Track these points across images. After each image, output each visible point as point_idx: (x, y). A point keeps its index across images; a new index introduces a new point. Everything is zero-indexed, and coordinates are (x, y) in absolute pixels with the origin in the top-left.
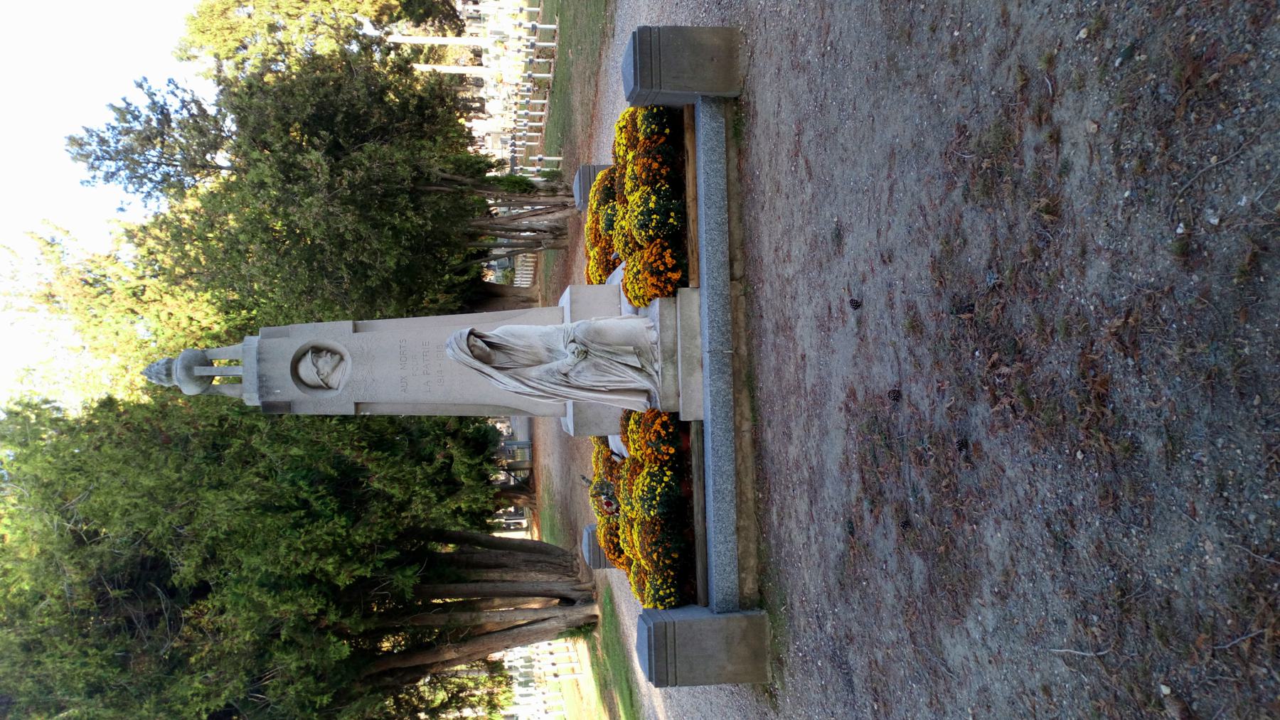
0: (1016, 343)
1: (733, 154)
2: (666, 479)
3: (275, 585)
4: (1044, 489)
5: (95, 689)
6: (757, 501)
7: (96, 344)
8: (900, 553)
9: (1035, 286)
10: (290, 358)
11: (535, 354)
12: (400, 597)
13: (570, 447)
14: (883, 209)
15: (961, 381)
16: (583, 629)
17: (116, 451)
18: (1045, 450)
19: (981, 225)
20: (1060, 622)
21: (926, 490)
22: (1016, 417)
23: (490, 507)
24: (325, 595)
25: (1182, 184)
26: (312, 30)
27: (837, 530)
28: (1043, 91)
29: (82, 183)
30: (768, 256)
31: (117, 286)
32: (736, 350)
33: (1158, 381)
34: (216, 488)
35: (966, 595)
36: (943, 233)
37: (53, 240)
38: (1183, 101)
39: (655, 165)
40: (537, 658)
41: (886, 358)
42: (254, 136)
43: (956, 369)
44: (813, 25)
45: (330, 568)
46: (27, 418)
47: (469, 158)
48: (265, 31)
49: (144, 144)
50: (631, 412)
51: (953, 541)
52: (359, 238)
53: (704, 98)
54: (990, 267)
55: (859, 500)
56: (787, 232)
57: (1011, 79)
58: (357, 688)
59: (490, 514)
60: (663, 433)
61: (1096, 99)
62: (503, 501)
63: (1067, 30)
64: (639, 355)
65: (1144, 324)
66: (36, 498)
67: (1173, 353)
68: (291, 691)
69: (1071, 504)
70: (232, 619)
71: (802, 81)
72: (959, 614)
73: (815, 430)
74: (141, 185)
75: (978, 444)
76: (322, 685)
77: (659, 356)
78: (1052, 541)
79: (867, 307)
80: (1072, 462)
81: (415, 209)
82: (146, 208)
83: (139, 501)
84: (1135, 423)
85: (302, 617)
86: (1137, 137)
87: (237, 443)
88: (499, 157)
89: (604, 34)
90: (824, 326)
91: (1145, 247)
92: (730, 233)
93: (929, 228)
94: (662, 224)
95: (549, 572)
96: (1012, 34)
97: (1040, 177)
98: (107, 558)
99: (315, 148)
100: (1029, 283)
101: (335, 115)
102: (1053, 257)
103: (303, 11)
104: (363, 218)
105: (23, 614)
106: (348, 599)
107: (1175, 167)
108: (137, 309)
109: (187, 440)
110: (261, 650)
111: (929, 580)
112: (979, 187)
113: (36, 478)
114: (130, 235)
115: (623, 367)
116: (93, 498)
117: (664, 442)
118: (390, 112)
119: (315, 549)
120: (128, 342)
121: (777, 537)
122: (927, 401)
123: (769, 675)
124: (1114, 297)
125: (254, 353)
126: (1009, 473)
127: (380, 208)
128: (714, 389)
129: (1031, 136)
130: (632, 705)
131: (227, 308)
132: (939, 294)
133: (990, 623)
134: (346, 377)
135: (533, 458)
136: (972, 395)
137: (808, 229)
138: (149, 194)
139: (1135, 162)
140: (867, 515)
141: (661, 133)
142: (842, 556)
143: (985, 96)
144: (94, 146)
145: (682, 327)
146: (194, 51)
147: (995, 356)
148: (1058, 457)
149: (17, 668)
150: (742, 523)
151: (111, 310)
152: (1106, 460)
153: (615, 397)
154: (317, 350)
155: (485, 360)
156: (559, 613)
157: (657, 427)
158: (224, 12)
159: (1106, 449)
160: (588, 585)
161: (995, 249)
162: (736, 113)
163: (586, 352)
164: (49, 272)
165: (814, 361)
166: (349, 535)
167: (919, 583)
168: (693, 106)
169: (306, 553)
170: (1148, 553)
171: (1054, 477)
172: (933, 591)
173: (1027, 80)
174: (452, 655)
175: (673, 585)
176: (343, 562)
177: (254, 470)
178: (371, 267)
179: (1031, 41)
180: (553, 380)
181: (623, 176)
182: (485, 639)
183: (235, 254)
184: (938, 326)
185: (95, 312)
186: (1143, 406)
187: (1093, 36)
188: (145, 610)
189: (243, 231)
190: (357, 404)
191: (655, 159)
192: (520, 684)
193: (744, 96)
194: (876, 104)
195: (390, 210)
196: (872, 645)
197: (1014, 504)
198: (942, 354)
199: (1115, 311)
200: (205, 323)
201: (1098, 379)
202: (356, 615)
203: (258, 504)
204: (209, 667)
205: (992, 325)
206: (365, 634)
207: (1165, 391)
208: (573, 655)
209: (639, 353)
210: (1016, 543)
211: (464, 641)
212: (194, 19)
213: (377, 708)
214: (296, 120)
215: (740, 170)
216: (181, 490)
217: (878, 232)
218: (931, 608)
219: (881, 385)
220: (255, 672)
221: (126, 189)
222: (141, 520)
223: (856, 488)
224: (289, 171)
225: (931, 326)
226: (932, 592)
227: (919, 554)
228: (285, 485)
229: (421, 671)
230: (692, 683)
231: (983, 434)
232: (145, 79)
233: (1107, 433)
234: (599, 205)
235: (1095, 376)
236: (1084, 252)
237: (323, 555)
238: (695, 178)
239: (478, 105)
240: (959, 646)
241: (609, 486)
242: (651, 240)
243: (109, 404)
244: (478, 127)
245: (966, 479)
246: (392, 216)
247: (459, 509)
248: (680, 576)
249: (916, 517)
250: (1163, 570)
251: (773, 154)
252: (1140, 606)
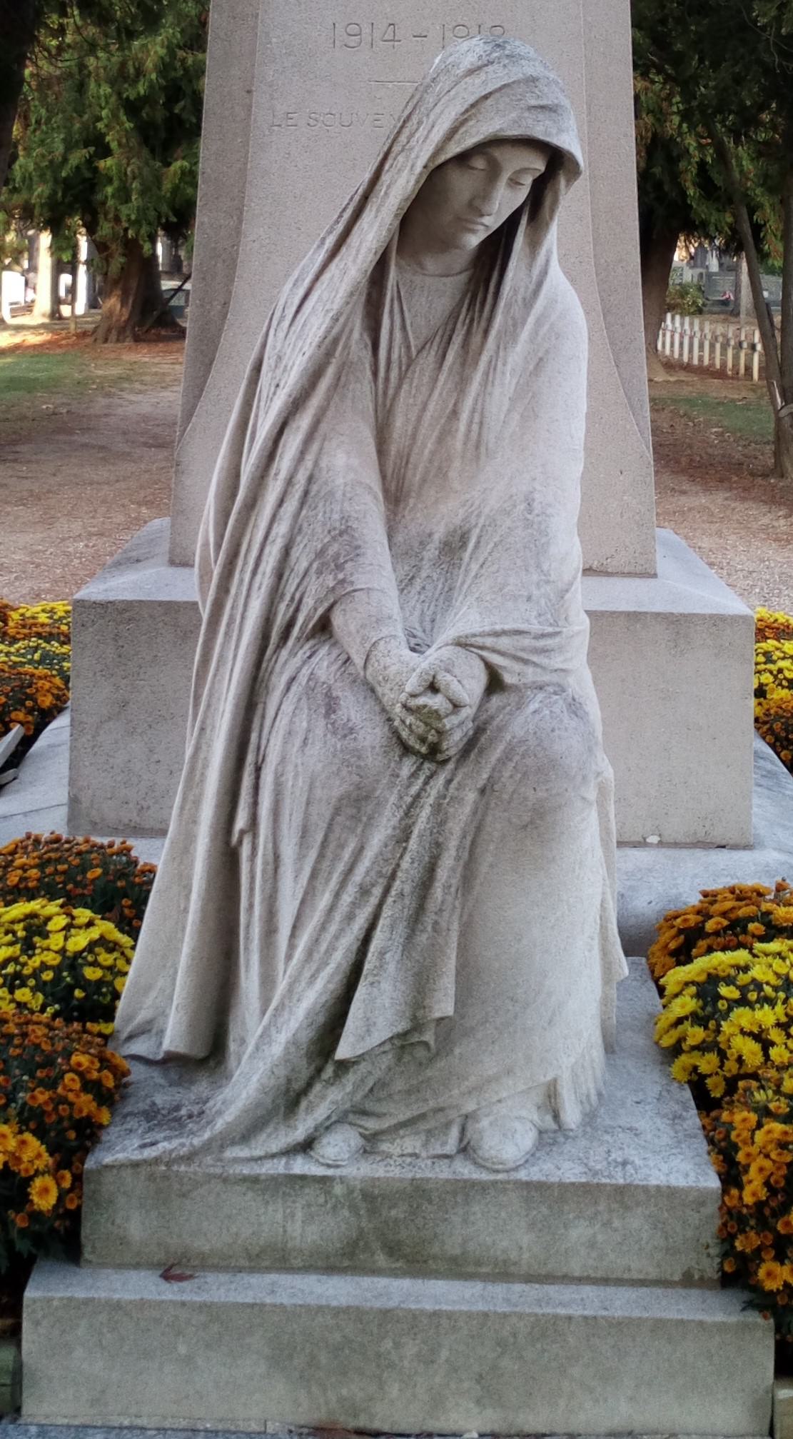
11: (440, 472)
64: (403, 1043)
77: (405, 1161)
115: (340, 957)
155: (420, 224)
163: (433, 753)
180: (301, 558)
209: (418, 1043)
247: (106, 152)
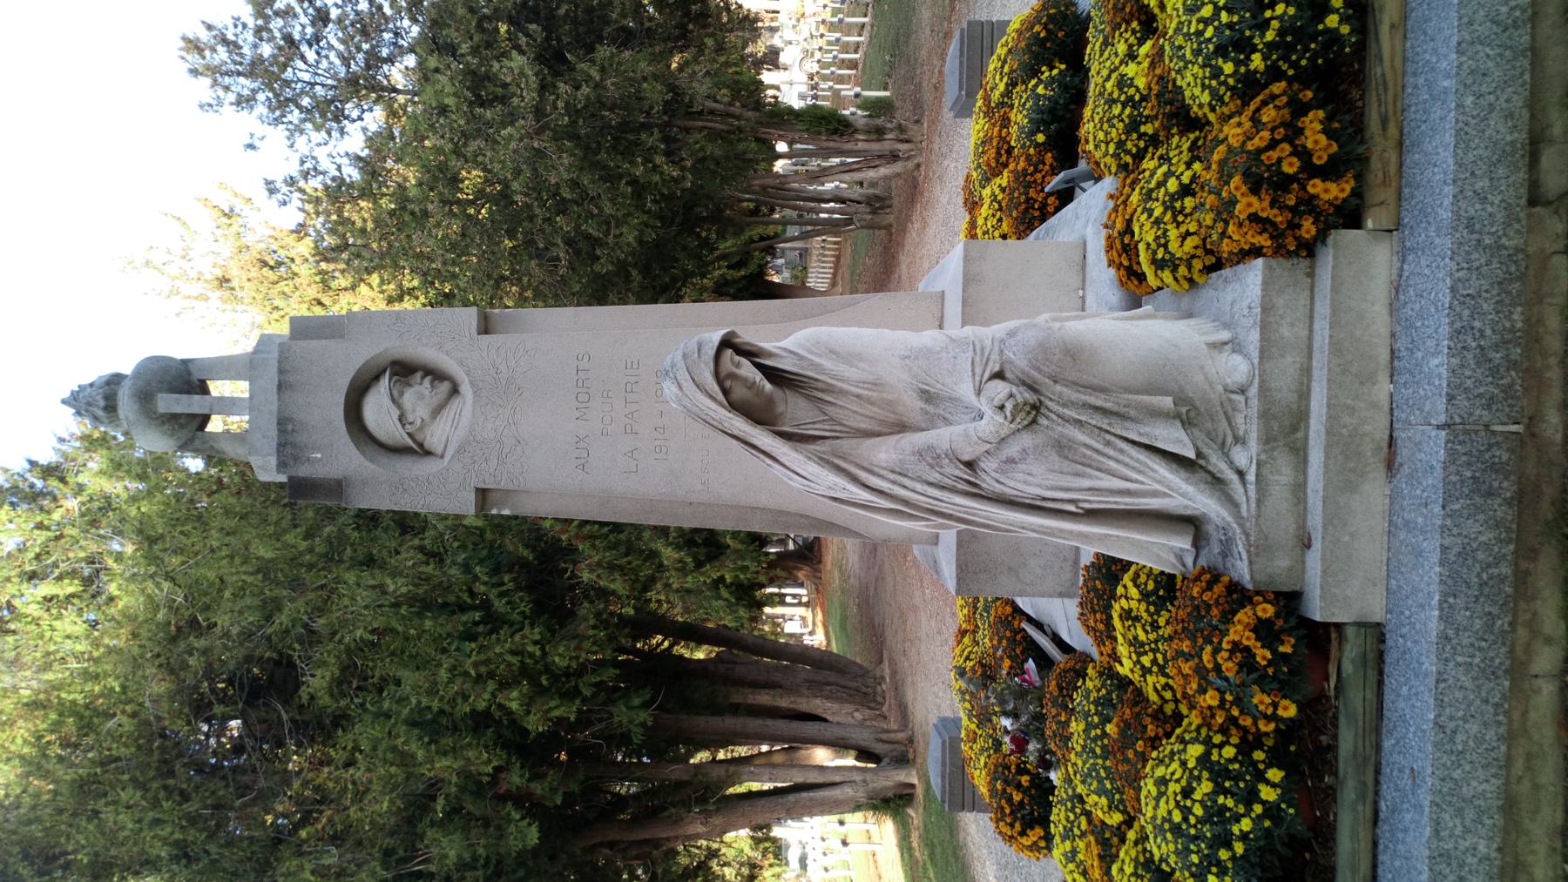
1: (695, 409)
2: (1267, 794)
3: (432, 726)
10: (344, 383)
11: (889, 404)
16: (893, 803)
29: (201, 106)
32: (1533, 421)
37: (232, 210)
45: (514, 705)
60: (1262, 655)
64: (1187, 423)
77: (1253, 432)
81: (668, 154)
92: (1535, 53)
95: (841, 700)
115: (1143, 456)
117: (1263, 682)
128: (1457, 545)
134: (461, 432)
145: (1336, 348)
149: (64, 817)
154: (404, 370)
155: (760, 414)
160: (901, 736)
163: (1036, 407)
164: (226, 248)
166: (544, 654)
169: (479, 680)
177: (416, 542)
180: (934, 476)
190: (483, 494)
195: (628, 150)
203: (411, 600)
209: (1187, 415)
216: (311, 566)
224: (482, 89)
234: (1012, 84)
237: (504, 685)
246: (632, 162)
247: (722, 579)
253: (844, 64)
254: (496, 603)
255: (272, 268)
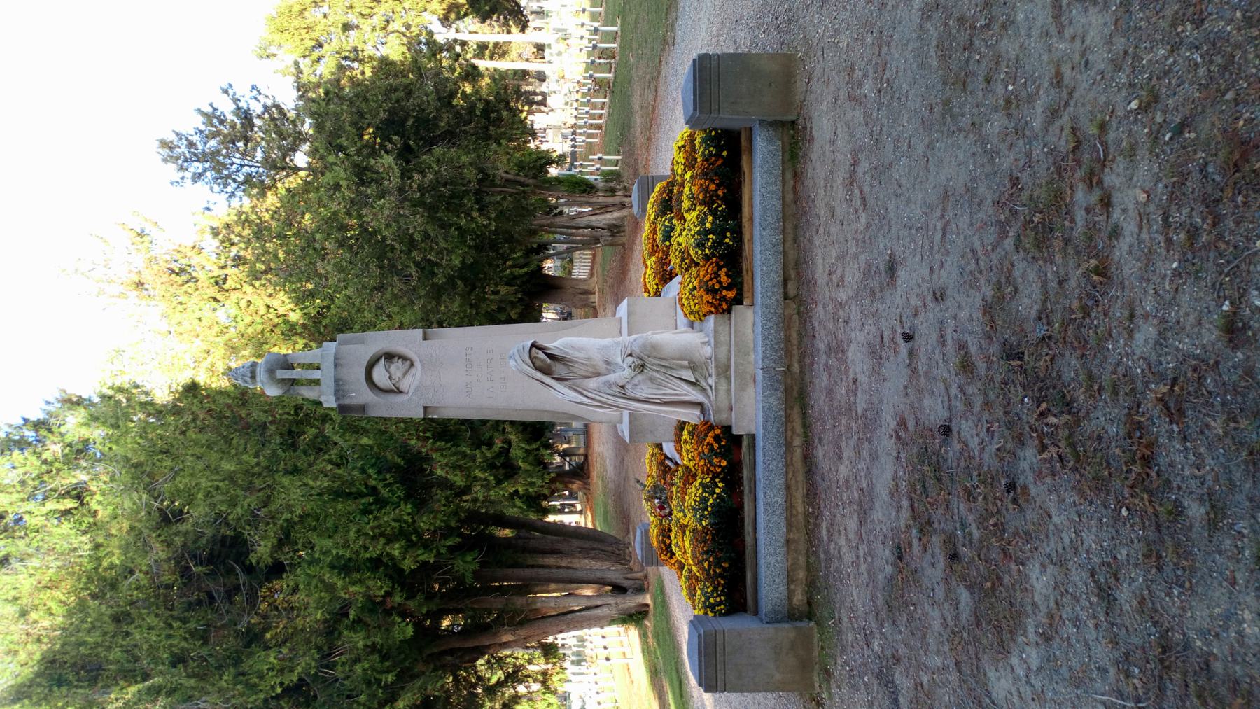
0: (1064, 396)
1: (789, 176)
2: (718, 490)
3: (345, 567)
4: (1089, 539)
5: (178, 660)
6: (807, 515)
7: (181, 329)
8: (947, 582)
9: (1084, 343)
10: (365, 363)
11: (594, 366)
12: (461, 580)
13: (622, 449)
14: (936, 248)
15: (1010, 425)
16: (635, 617)
17: (200, 436)
18: (1091, 502)
19: (1032, 276)
20: (1103, 670)
21: (973, 525)
22: (1063, 467)
23: (546, 492)
24: (391, 578)
25: (1228, 262)
26: (384, 29)
27: (886, 553)
28: (1094, 155)
30: (822, 280)
31: (201, 275)
33: (1202, 450)
34: (291, 473)
35: (1011, 632)
36: (994, 279)
38: (1231, 182)
39: (712, 187)
40: (590, 639)
41: (937, 393)
42: (330, 140)
43: (1005, 413)
44: (870, 60)
45: (396, 553)
46: (119, 402)
47: (531, 153)
48: (339, 30)
49: (228, 144)
50: (684, 423)
51: (999, 578)
52: (426, 237)
53: (762, 122)
54: (1040, 319)
55: (908, 527)
56: (841, 257)
57: (1064, 138)
58: (420, 667)
59: (546, 498)
60: (716, 446)
61: (1145, 169)
62: (558, 485)
63: (1119, 98)
64: (693, 370)
65: (1189, 393)
66: (125, 476)
67: (1217, 426)
68: (358, 669)
69: (1115, 558)
70: (304, 598)
71: (858, 114)
72: (1003, 650)
73: (865, 453)
74: (226, 185)
75: (1025, 488)
76: (387, 664)
77: (712, 371)
78: (1096, 591)
79: (919, 342)
80: (1117, 518)
81: (480, 210)
82: (224, 205)
83: (221, 484)
84: (1179, 488)
85: (369, 598)
86: (1185, 211)
87: (312, 431)
88: (559, 152)
89: (664, 41)
90: (876, 352)
91: (1192, 318)
93: (981, 272)
94: (718, 244)
95: (602, 560)
96: (1065, 95)
97: (1090, 238)
98: (191, 537)
99: (387, 152)
100: (1077, 338)
101: (406, 119)
102: (1101, 316)
103: (376, 10)
104: (432, 219)
105: (113, 586)
106: (410, 582)
107: (1222, 246)
108: (219, 296)
109: (264, 426)
110: (331, 629)
111: (975, 612)
112: (1031, 240)
113: (127, 459)
114: (215, 232)
116: (178, 479)
118: (457, 115)
119: (382, 534)
120: (210, 327)
121: (827, 552)
122: (976, 440)
123: (817, 685)
124: (1161, 364)
125: (332, 358)
126: (1056, 519)
127: (447, 209)
129: (1082, 197)
130: (682, 696)
131: (301, 299)
132: (990, 337)
133: (1035, 663)
134: (416, 383)
135: (588, 444)
136: (1020, 440)
137: (862, 257)
138: (232, 195)
139: (1183, 236)
140: (915, 542)
141: (718, 155)
142: (890, 579)
143: (1038, 152)
144: (184, 149)
145: (737, 344)
146: (273, 50)
147: (1044, 406)
148: (1104, 511)
149: (107, 638)
150: (792, 536)
151: (195, 299)
152: (1150, 520)
153: (669, 410)
154: (390, 356)
155: (546, 371)
156: (611, 601)
157: (710, 439)
158: (302, 12)
159: (1150, 510)
160: (640, 575)
161: (1045, 301)
162: (793, 137)
163: (643, 366)
164: (139, 261)
165: (866, 386)
166: (414, 522)
167: (966, 615)
168: (751, 129)
170: (1189, 614)
171: (1100, 528)
172: (978, 624)
173: (1079, 142)
174: (508, 637)
175: (723, 593)
176: (409, 546)
177: (327, 457)
178: (436, 264)
179: (1083, 105)
181: (681, 194)
182: (540, 623)
183: (311, 252)
184: (988, 369)
185: (180, 299)
186: (1187, 472)
187: (1145, 108)
188: (225, 585)
189: (319, 230)
190: (425, 408)
191: (712, 181)
192: (573, 662)
193: (801, 120)
194: (931, 146)
196: (918, 668)
197: (1060, 550)
198: (992, 397)
199: (1162, 377)
200: (281, 311)
201: (1143, 440)
202: (419, 597)
203: (329, 491)
204: (284, 642)
205: (1041, 375)
206: (428, 615)
207: (1209, 461)
208: (625, 639)
209: (693, 367)
210: (1061, 587)
211: (521, 624)
212: (273, 19)
213: (439, 685)
214: (369, 125)
215: (795, 193)
216: (259, 474)
217: (931, 269)
218: (976, 640)
219: (932, 418)
220: (325, 648)
221: (211, 189)
222: (222, 502)
223: (905, 514)
224: (362, 174)
225: (981, 366)
226: (978, 625)
227: (966, 587)
228: (355, 472)
229: (479, 652)
230: (740, 689)
231: (1031, 478)
232: (231, 86)
233: (1151, 495)
234: (657, 215)
235: (1141, 438)
236: (1132, 316)
237: (390, 540)
238: (751, 199)
239: (540, 98)
240: (1003, 680)
241: (662, 490)
242: (707, 258)
243: (192, 389)
244: (538, 120)
245: (1014, 521)
246: (458, 217)
247: (517, 492)
248: (730, 584)
249: (964, 550)
250: (1203, 633)
251: (829, 181)
252: (1180, 664)
253: (591, 126)
254: (382, 491)
255: (178, 274)
